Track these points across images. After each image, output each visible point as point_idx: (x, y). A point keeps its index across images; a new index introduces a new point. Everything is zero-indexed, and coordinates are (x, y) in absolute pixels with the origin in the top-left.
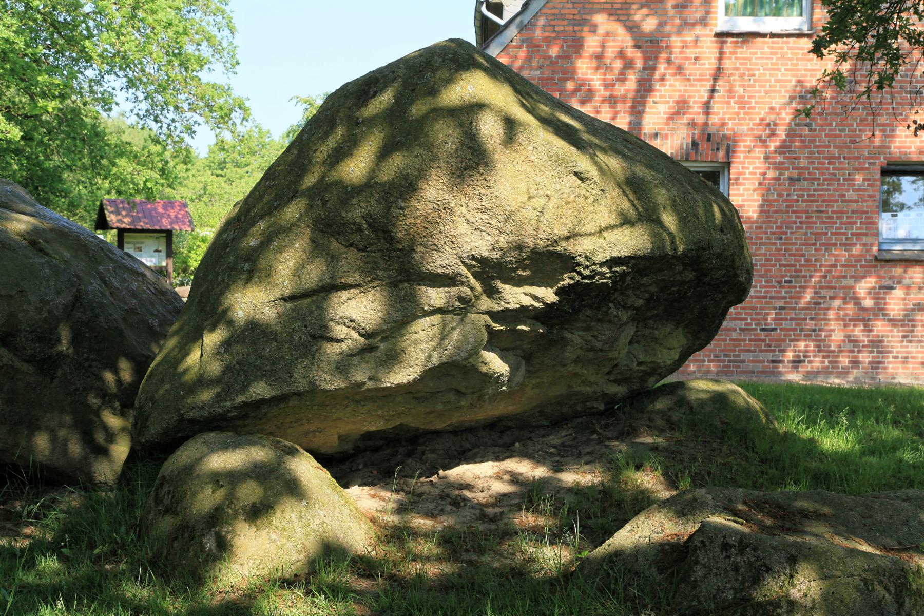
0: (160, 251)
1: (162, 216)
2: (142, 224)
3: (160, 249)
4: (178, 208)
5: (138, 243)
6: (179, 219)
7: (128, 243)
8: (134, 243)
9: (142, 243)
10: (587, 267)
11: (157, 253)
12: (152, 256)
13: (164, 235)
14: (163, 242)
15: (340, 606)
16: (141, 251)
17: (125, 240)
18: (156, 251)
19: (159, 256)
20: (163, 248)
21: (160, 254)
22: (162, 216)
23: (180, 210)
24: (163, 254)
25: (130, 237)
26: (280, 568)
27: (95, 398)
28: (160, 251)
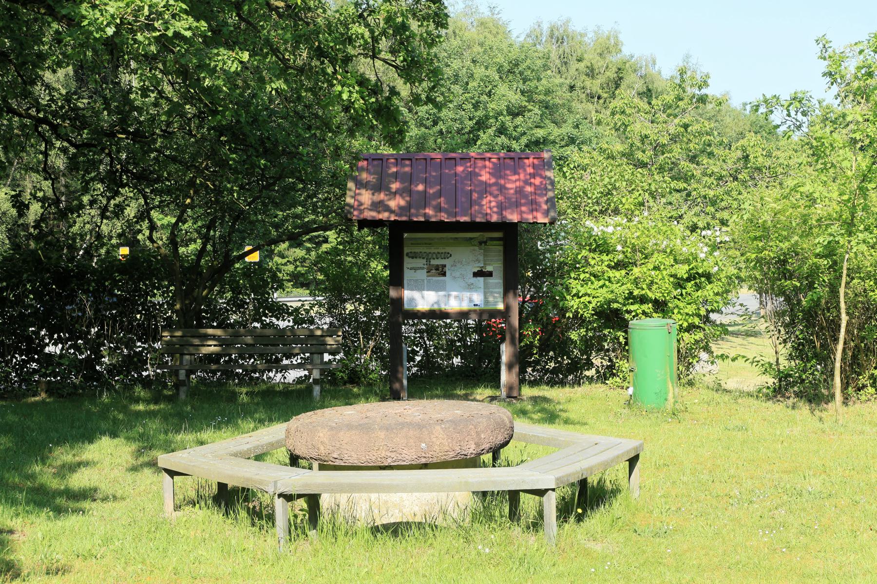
0: (490, 274)
1: (485, 189)
2: (430, 211)
3: (489, 268)
4: (530, 170)
5: (438, 256)
6: (525, 196)
7: (414, 256)
8: (428, 257)
9: (447, 256)
10: (428, 119)
11: (481, 279)
12: (470, 287)
13: (498, 235)
14: (497, 250)
15: (7, 206)
16: (444, 274)
17: (406, 250)
18: (478, 274)
19: (485, 284)
20: (495, 266)
21: (490, 280)
22: (485, 189)
23: (533, 176)
24: (497, 281)
25: (416, 243)
26: (341, 537)
27: (149, 376)
28: (490, 274)
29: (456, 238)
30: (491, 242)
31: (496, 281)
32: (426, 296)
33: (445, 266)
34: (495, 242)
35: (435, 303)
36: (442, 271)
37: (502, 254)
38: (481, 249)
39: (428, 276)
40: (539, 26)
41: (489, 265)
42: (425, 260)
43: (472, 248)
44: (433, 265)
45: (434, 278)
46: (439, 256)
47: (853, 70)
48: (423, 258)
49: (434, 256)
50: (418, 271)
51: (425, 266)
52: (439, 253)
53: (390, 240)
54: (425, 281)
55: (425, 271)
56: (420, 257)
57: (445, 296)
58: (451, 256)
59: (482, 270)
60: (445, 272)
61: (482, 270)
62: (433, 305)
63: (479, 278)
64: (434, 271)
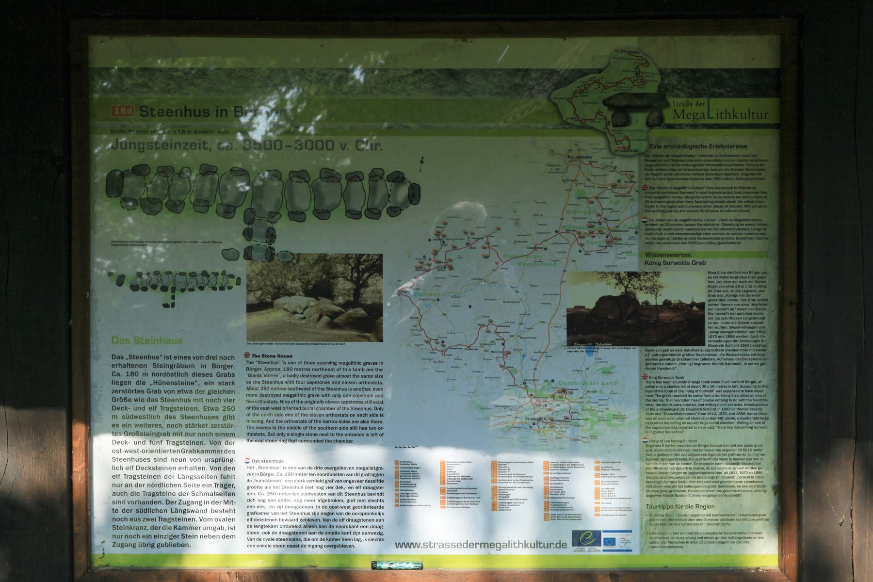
29: (452, 74)
30: (697, 107)
31: (730, 373)
32: (241, 474)
33: (376, 266)
34: (720, 105)
35: (310, 523)
36: (355, 302)
37: (768, 185)
38: (626, 152)
39: (256, 336)
40: (444, 242)
41: (683, 260)
42: (238, 223)
43: (562, 142)
44: (291, 260)
45: (301, 351)
46: (331, 193)
47: (597, 239)
48: (228, 212)
49: (303, 200)
50: (181, 298)
51: (241, 268)
52: (329, 175)
53: (354, 296)
54: (239, 367)
55: (239, 296)
56: (202, 205)
57: (377, 475)
58: (414, 195)
59: (628, 299)
60: (376, 311)
61: (628, 299)
62: (294, 539)
63: (610, 354)
64: (300, 300)
